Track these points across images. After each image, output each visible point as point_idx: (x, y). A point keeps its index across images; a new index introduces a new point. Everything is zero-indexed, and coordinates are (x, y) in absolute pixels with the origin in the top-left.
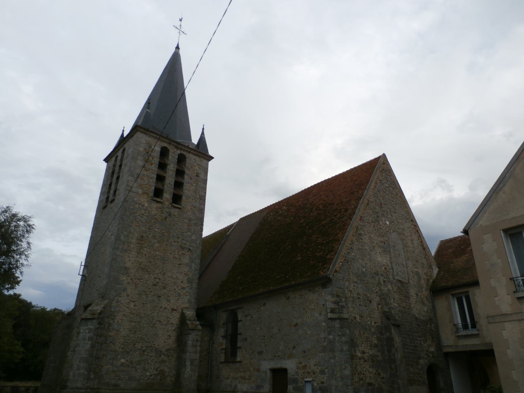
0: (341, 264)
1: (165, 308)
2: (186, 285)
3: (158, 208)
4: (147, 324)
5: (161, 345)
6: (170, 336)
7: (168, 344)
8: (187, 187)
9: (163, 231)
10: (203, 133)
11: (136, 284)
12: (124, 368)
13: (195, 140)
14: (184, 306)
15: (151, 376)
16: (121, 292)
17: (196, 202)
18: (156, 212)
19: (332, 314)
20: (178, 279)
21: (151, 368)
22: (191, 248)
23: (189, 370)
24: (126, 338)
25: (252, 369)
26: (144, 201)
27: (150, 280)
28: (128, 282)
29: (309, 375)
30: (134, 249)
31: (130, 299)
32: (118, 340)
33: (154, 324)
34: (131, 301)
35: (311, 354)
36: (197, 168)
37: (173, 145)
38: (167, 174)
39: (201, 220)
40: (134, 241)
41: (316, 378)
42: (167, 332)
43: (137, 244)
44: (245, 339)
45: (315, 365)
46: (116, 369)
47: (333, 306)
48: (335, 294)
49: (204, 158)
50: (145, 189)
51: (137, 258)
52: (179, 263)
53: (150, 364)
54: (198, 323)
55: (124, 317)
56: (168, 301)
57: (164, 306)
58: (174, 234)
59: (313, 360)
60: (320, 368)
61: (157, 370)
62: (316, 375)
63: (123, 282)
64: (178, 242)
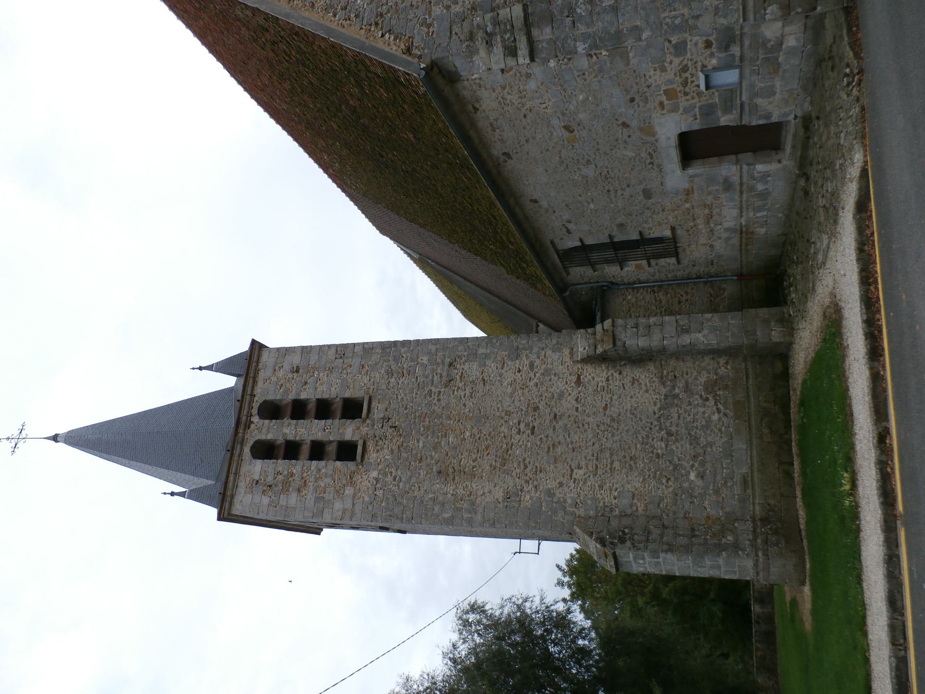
0: (387, 35)
1: (577, 400)
2: (525, 361)
3: (377, 447)
4: (613, 435)
5: (652, 398)
6: (633, 381)
7: (649, 381)
8: (325, 389)
9: (422, 429)
10: (210, 368)
11: (536, 472)
12: (708, 471)
13: (229, 381)
14: (568, 359)
15: (719, 411)
16: (555, 500)
17: (351, 366)
18: (386, 450)
19: (520, 53)
20: (515, 380)
21: (704, 413)
22: (447, 361)
23: (700, 336)
24: (646, 477)
25: (688, 205)
26: (367, 478)
27: (523, 442)
28: (533, 489)
29: (689, 81)
30: (467, 487)
31: (568, 479)
32: (651, 493)
33: (613, 420)
34: (571, 476)
35: (637, 84)
36: (281, 374)
37: (244, 434)
38: (305, 438)
39: (387, 348)
40: (450, 489)
41: (696, 63)
42: (626, 388)
43: (456, 481)
44: (621, 226)
45: (663, 70)
46: (711, 488)
47: (498, 50)
48: (468, 46)
49: (258, 362)
50: (344, 482)
51: (484, 478)
52: (482, 383)
53: (694, 416)
54: (599, 327)
55: (605, 488)
56: (561, 395)
57: (574, 402)
58: (424, 405)
59: (650, 77)
60: (668, 56)
61: (707, 399)
62: (690, 64)
63: (534, 499)
64: (440, 392)
